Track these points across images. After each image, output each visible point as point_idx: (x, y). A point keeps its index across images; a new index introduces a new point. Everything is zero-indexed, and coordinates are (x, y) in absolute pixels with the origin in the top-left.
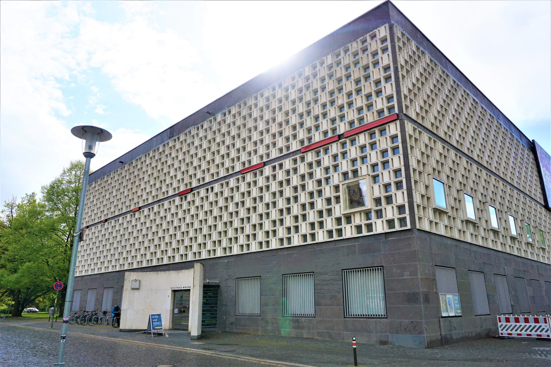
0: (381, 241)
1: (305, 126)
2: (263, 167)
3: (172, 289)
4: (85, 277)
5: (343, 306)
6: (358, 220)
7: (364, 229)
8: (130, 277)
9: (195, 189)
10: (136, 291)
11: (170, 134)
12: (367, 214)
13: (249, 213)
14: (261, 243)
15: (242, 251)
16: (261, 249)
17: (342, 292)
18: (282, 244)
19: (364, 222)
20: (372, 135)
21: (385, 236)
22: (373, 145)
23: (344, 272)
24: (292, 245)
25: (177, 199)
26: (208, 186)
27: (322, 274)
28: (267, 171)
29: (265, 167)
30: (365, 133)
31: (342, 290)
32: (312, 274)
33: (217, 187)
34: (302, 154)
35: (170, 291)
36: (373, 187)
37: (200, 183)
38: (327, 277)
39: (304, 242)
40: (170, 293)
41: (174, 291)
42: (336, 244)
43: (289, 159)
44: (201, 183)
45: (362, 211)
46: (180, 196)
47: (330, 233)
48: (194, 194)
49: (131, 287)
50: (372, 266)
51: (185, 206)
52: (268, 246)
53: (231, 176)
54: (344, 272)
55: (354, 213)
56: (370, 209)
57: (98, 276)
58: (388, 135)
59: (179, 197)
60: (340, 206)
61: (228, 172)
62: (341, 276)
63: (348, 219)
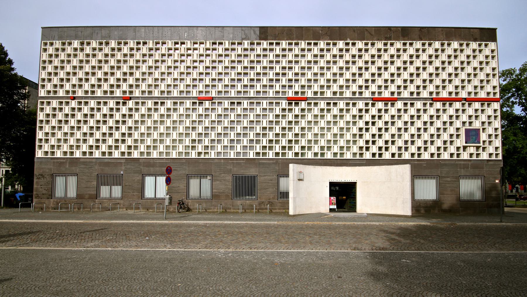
2: (396, 101)
3: (330, 181)
10: (301, 181)
12: (478, 148)
28: (399, 105)
29: (398, 102)
41: (330, 183)
46: (288, 101)
59: (286, 101)
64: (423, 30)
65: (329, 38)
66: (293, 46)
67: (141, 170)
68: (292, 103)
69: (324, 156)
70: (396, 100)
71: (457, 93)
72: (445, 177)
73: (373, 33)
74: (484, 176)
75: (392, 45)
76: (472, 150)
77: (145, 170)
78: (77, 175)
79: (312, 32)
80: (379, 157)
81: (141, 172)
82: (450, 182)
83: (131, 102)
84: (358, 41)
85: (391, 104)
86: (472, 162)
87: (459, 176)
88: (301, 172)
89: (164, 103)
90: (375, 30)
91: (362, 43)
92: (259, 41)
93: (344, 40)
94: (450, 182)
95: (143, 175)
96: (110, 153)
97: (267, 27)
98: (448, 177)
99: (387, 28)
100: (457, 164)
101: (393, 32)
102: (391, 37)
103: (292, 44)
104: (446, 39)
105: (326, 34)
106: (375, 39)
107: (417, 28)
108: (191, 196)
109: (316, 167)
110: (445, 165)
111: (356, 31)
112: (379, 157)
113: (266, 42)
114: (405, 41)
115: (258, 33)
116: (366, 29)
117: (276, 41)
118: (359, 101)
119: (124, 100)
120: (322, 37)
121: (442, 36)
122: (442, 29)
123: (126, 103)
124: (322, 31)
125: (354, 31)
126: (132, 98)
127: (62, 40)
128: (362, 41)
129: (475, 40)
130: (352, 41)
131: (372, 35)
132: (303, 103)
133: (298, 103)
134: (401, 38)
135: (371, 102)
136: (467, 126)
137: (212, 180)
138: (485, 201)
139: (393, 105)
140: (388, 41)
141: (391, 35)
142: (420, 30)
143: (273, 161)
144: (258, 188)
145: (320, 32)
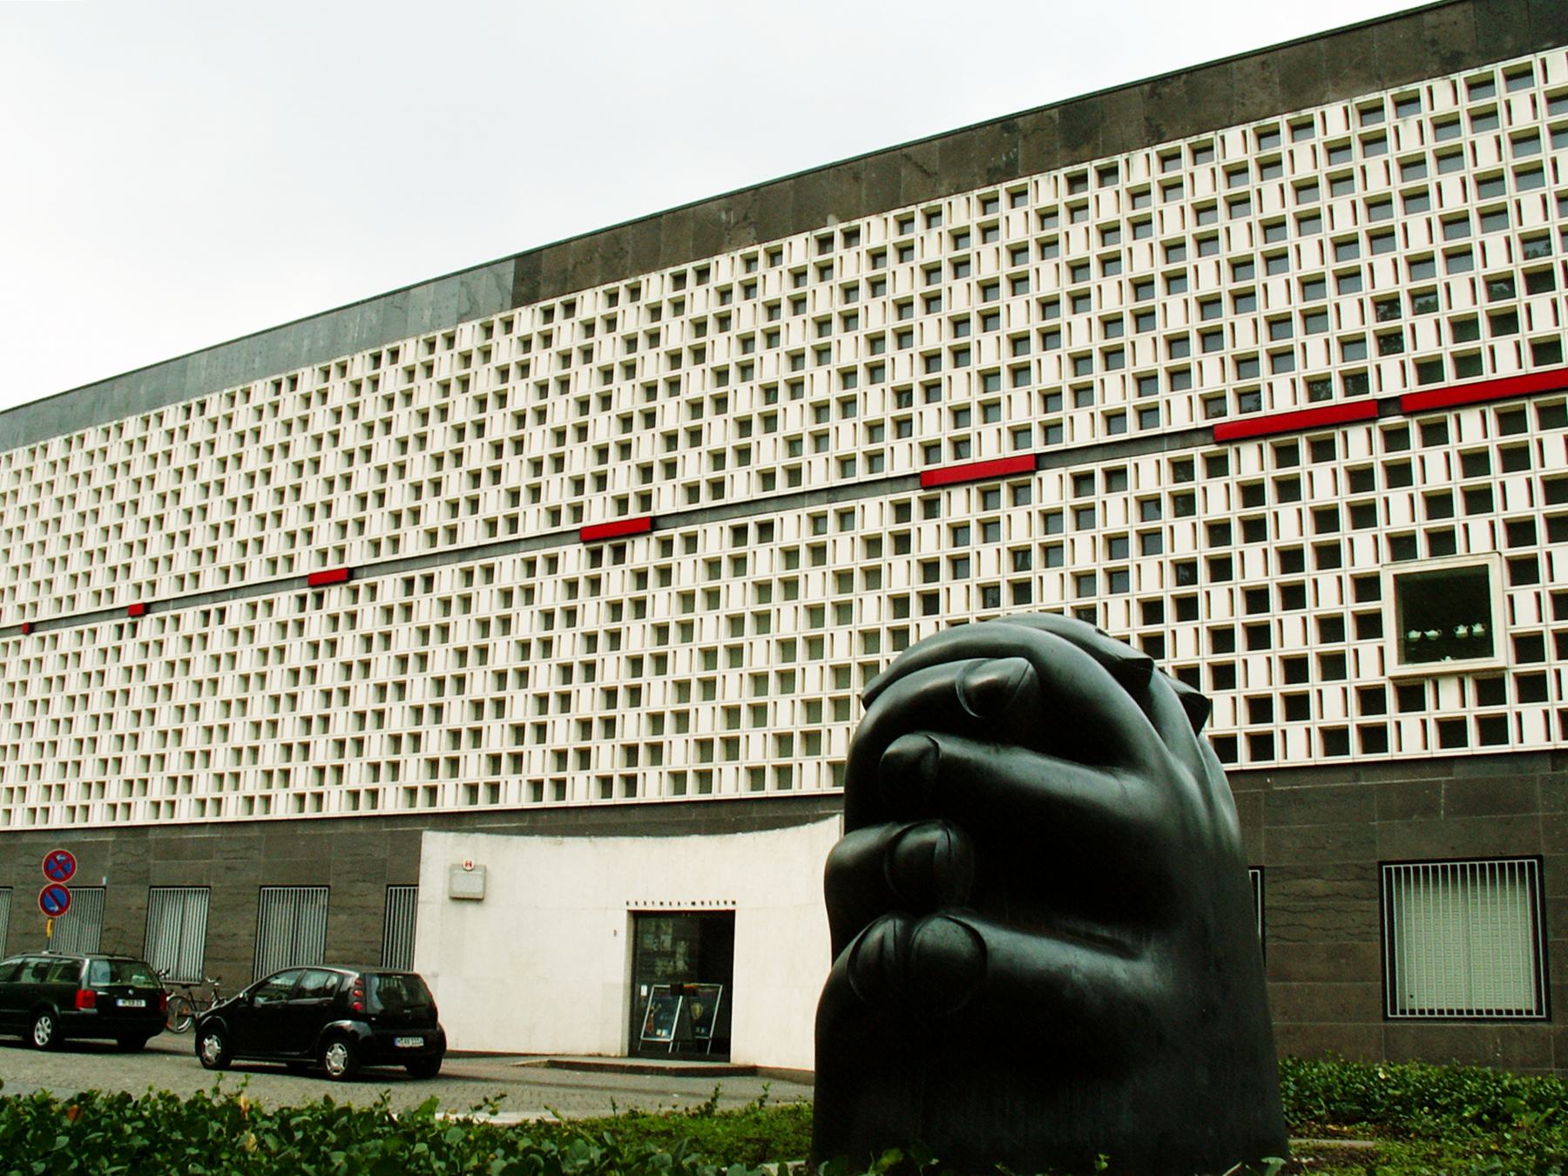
0: (1537, 775)
1: (707, 445)
2: (1033, 472)
3: (633, 907)
4: (151, 830)
5: (1380, 983)
6: (1450, 702)
7: (770, 778)
8: (438, 849)
9: (365, 572)
10: (470, 908)
11: (518, 280)
12: (1490, 689)
13: (328, 705)
14: (355, 795)
15: (301, 810)
16: (471, 804)
17: (1379, 937)
18: (474, 800)
19: (1472, 711)
20: (988, 498)
21: (1553, 764)
22: (989, 528)
23: (1389, 871)
24: (439, 809)
25: (574, 560)
26: (213, 603)
27: (1297, 876)
28: (1052, 488)
29: (1040, 474)
30: (1263, 442)
31: (1378, 930)
32: (1531, 865)
33: (448, 580)
34: (1213, 448)
35: (625, 914)
36: (1511, 598)
37: (182, 590)
38: (1318, 885)
39: (557, 799)
40: (622, 925)
41: (637, 916)
42: (1357, 779)
43: (799, 511)
44: (189, 590)
45: (1467, 673)
46: (585, 542)
47: (756, 774)
48: (355, 592)
49: (451, 888)
50: (1498, 855)
51: (132, 656)
52: (433, 802)
53: (236, 592)
54: (1389, 871)
55: (1435, 679)
56: (1504, 669)
57: (110, 838)
58: (1036, 506)
59: (581, 546)
60: (1381, 650)
61: (377, 554)
62: (1376, 885)
63: (1411, 696)
64: (1167, 90)
65: (753, 232)
66: (1501, 93)
67: (148, 871)
68: (1522, 413)
69: (1383, 748)
70: (1038, 462)
71: (1051, 430)
72: (1296, 875)
73: (935, 164)
74: (1261, 868)
75: (1017, 196)
76: (1450, 702)
77: (161, 870)
78: (200, 887)
79: (692, 224)
80: (1255, 757)
81: (148, 878)
82: (1323, 903)
83: (1049, 476)
84: (867, 219)
85: (1015, 489)
86: (1459, 773)
87: (1381, 864)
88: (469, 867)
89: (1122, 472)
90: (942, 149)
91: (886, 219)
92: (990, 189)
93: (811, 229)
94: (1323, 903)
95: (388, 886)
96: (1374, 738)
97: (538, 251)
98: (1313, 873)
99: (999, 125)
100: (1364, 793)
101: (1025, 137)
102: (1016, 159)
103: (1490, 82)
104: (1284, 103)
105: (745, 218)
106: (943, 190)
107: (1137, 89)
108: (1402, 1002)
109: (568, 840)
110: (1297, 798)
111: (863, 175)
112: (1254, 758)
113: (530, 309)
114: (1077, 168)
115: (509, 279)
116: (906, 156)
117: (1097, 162)
118: (862, 502)
119: (926, 488)
120: (727, 238)
121: (1262, 96)
122: (1263, 57)
123: (1223, 459)
124: (728, 211)
125: (857, 178)
126: (661, 522)
127: (288, 371)
128: (885, 215)
129: (1450, 64)
130: (845, 225)
131: (927, 174)
132: (1357, 434)
133: (1443, 425)
134: (1061, 154)
135: (914, 496)
136: (1424, 562)
137: (330, 909)
138: (1549, 1019)
139: (1323, 451)
140: (998, 187)
141: (1016, 155)
142: (1153, 93)
143: (521, 820)
144: (1378, 944)
145: (724, 216)
